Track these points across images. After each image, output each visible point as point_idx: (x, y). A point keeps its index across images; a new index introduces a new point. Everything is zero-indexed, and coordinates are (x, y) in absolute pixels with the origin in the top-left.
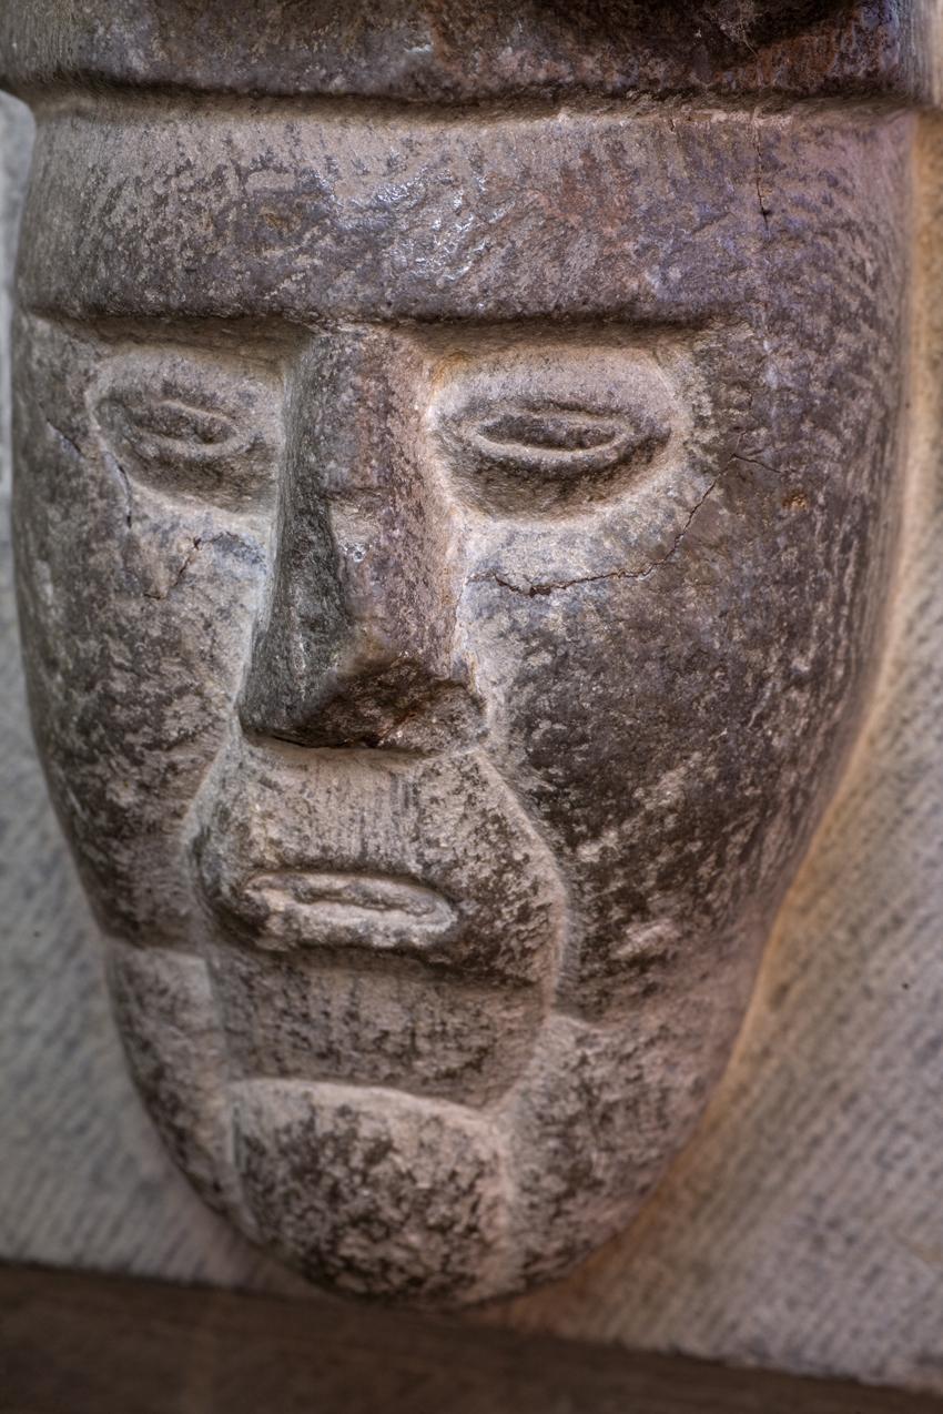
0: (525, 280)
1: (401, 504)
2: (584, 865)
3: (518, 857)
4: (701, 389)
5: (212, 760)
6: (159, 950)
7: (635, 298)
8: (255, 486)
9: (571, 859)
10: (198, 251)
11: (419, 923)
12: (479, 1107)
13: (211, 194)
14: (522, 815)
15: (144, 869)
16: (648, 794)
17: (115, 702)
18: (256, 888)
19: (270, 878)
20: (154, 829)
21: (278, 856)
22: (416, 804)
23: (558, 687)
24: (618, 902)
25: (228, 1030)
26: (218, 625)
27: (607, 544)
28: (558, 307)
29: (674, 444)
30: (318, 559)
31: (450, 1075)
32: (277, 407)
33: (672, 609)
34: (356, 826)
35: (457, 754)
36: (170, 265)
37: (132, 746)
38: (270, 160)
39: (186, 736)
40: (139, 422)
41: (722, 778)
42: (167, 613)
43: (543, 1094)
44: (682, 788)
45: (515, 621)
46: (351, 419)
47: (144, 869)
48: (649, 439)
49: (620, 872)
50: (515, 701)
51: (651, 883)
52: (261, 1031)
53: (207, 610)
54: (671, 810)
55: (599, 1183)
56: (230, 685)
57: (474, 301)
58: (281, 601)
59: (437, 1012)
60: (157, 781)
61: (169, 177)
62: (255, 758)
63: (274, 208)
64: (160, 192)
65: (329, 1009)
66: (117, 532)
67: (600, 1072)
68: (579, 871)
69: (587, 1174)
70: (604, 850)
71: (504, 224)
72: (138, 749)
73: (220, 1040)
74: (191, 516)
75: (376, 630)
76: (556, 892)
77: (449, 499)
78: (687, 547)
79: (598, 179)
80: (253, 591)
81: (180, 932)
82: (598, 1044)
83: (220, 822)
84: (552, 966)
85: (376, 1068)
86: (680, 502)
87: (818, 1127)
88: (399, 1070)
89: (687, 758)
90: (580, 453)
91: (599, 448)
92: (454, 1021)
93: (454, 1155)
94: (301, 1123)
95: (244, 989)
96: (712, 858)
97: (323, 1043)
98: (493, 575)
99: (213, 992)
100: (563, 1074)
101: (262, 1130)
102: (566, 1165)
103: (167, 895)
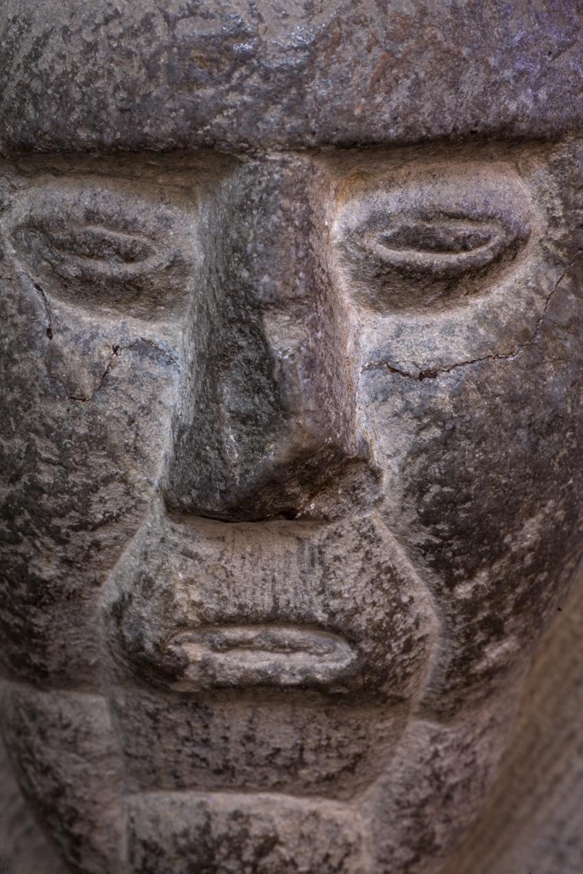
0: (428, 107)
1: (321, 309)
2: (459, 601)
3: (405, 599)
4: (554, 193)
5: (132, 536)
6: (62, 692)
7: (515, 119)
8: (169, 297)
9: (448, 598)
10: (131, 93)
11: (321, 662)
12: (347, 800)
13: (141, 41)
14: (408, 564)
15: (60, 629)
16: (514, 539)
17: (42, 491)
18: (177, 643)
19: (190, 634)
20: (74, 596)
21: (199, 615)
22: (322, 563)
23: (448, 456)
24: (482, 628)
25: (127, 754)
26: (140, 421)
27: (481, 331)
28: (455, 129)
29: (533, 242)
30: (249, 362)
31: (330, 778)
32: (193, 227)
33: (536, 383)
34: (268, 585)
35: (357, 518)
36: (103, 106)
37: (59, 528)
38: (197, 7)
39: (111, 517)
40: (61, 246)
41: (567, 519)
42: (94, 412)
43: (401, 785)
44: (539, 531)
45: (408, 403)
46: (282, 237)
47: (60, 629)
48: (517, 239)
49: (487, 604)
50: (408, 471)
51: (509, 610)
52: (163, 755)
53: (130, 408)
54: (530, 549)
55: (438, 847)
56: (152, 471)
57: (386, 127)
58: (206, 398)
59: (324, 729)
60: (81, 557)
61: (98, 26)
62: (177, 534)
63: (204, 51)
64: (90, 39)
65: (228, 734)
66: (38, 344)
67: (446, 762)
68: (454, 606)
69: (430, 842)
70: (476, 588)
71: (408, 57)
72: (64, 531)
73: (119, 763)
74: (110, 326)
75: (308, 422)
76: (433, 625)
77: (347, 300)
78: (545, 330)
79: (480, 15)
80: (169, 389)
81: (86, 677)
82: (447, 740)
83: (144, 589)
84: (419, 688)
85: (266, 778)
86: (538, 291)
87: (559, 768)
88: (286, 778)
89: (544, 506)
90: (464, 255)
91: (479, 250)
92: (338, 735)
93: (328, 841)
94: (198, 828)
95: (150, 722)
96: (551, 584)
97: (220, 762)
98: (385, 364)
99: (113, 724)
100: (419, 767)
101: (160, 835)
102: (416, 838)
103: (80, 649)
